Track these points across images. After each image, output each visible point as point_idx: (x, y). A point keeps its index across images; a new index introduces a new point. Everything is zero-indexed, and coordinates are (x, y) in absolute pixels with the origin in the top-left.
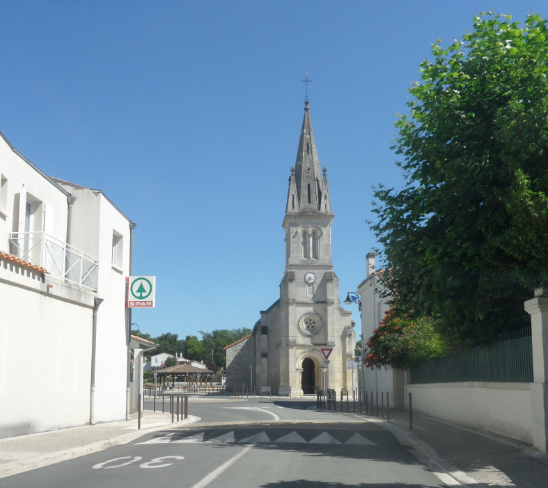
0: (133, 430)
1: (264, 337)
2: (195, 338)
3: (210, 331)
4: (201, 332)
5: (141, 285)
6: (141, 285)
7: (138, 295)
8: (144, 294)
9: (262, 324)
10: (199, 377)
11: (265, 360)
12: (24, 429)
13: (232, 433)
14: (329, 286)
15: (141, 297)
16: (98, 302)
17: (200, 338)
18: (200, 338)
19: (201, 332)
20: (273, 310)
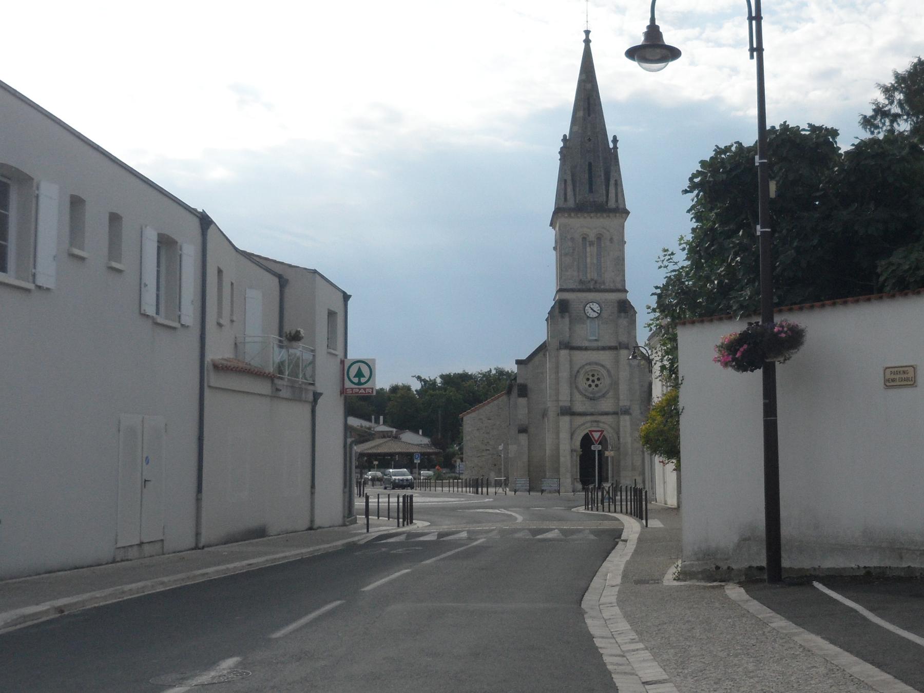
0: (362, 534)
1: (522, 401)
2: (408, 388)
3: (433, 373)
4: (419, 378)
5: (359, 369)
6: (359, 369)
7: (356, 380)
8: (363, 380)
9: (519, 381)
10: (417, 461)
11: (523, 438)
12: (260, 533)
13: (466, 532)
14: (578, 374)
15: (359, 383)
16: (317, 396)
17: (416, 386)
18: (416, 386)
19: (419, 378)
20: (537, 359)
